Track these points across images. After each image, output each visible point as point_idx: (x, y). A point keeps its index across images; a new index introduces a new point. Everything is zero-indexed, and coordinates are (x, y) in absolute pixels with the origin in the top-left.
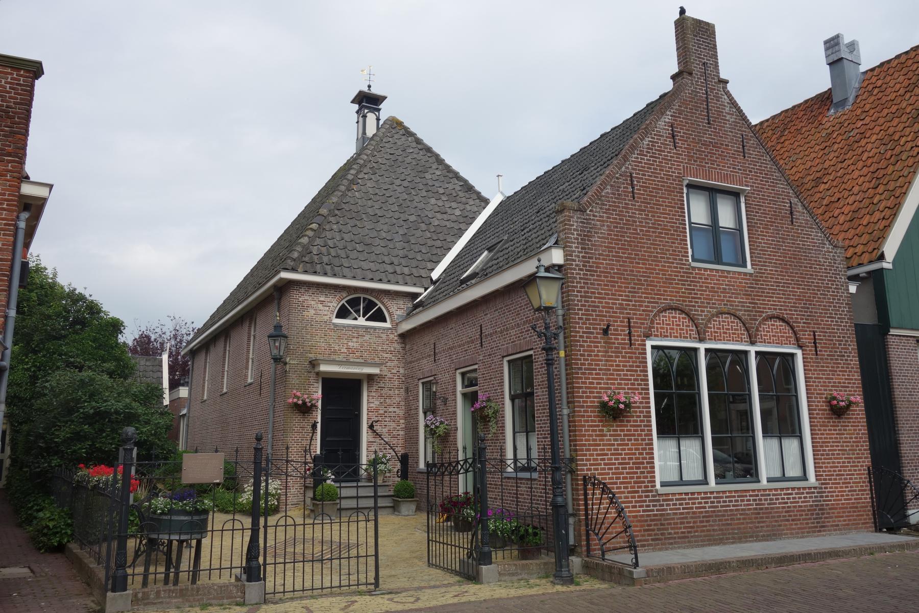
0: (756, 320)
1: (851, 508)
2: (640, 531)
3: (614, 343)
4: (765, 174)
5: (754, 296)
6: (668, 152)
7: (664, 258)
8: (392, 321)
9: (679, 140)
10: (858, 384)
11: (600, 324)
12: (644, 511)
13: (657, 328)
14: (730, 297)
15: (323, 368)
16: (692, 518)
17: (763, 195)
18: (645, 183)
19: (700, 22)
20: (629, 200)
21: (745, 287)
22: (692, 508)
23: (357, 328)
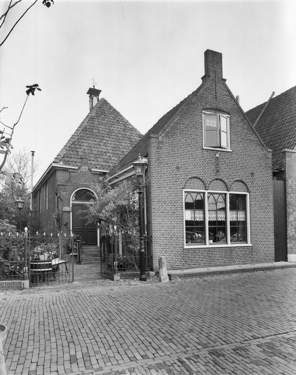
10: (273, 225)
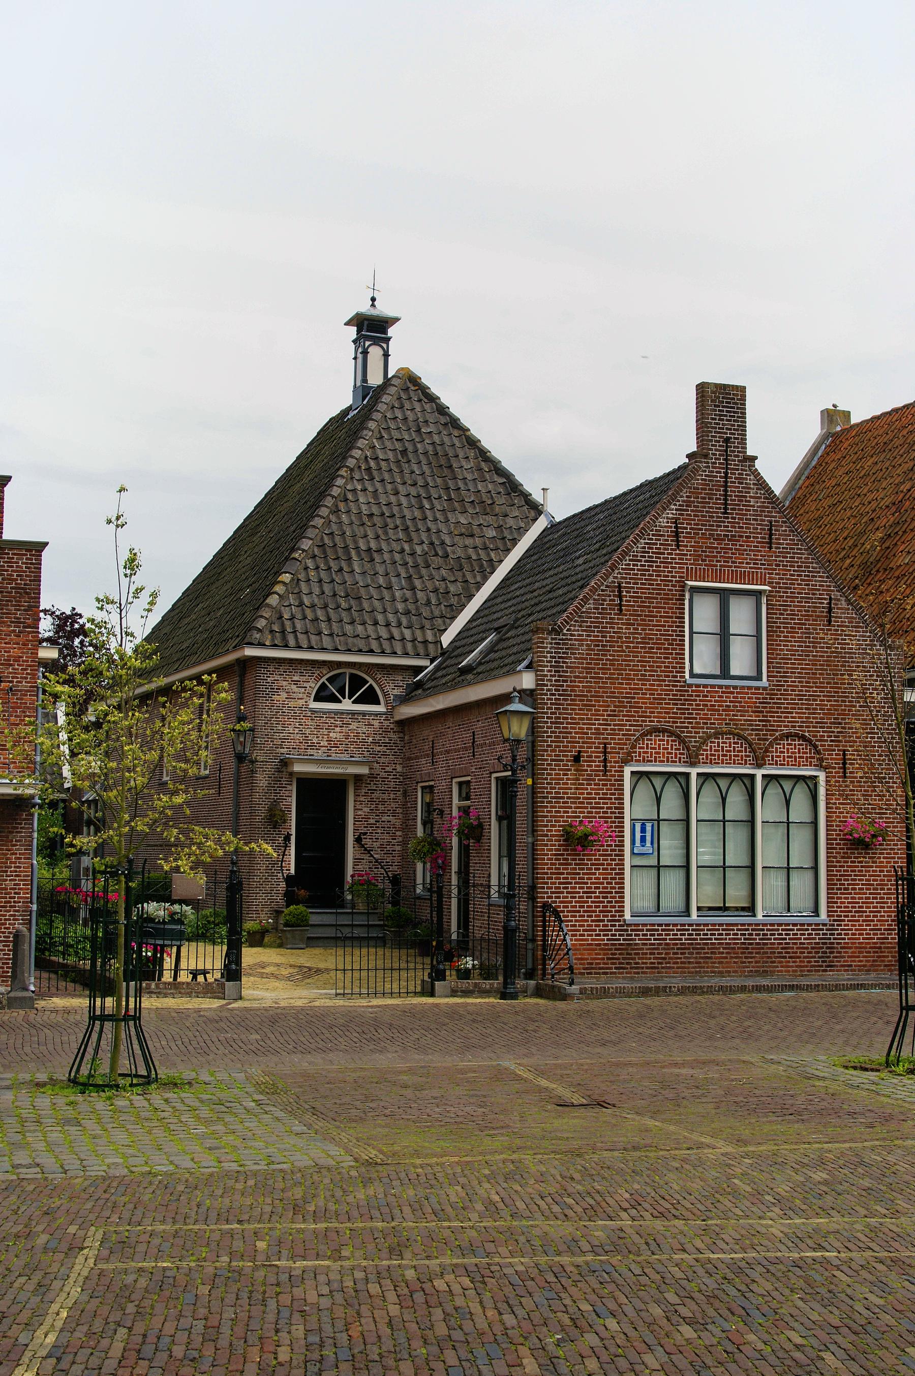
0: (767, 740)
1: (871, 948)
2: (603, 959)
3: (587, 770)
4: (798, 567)
5: (767, 712)
6: (668, 554)
7: (653, 676)
8: (387, 704)
9: (684, 537)
11: (571, 751)
12: (608, 940)
13: (640, 752)
14: (734, 715)
15: (298, 768)
16: (664, 949)
17: (791, 593)
18: (637, 593)
19: (725, 387)
20: (615, 614)
21: (756, 703)
22: (666, 939)
23: (342, 713)
